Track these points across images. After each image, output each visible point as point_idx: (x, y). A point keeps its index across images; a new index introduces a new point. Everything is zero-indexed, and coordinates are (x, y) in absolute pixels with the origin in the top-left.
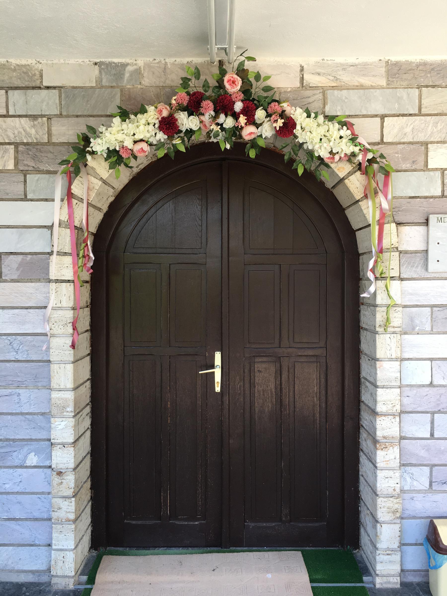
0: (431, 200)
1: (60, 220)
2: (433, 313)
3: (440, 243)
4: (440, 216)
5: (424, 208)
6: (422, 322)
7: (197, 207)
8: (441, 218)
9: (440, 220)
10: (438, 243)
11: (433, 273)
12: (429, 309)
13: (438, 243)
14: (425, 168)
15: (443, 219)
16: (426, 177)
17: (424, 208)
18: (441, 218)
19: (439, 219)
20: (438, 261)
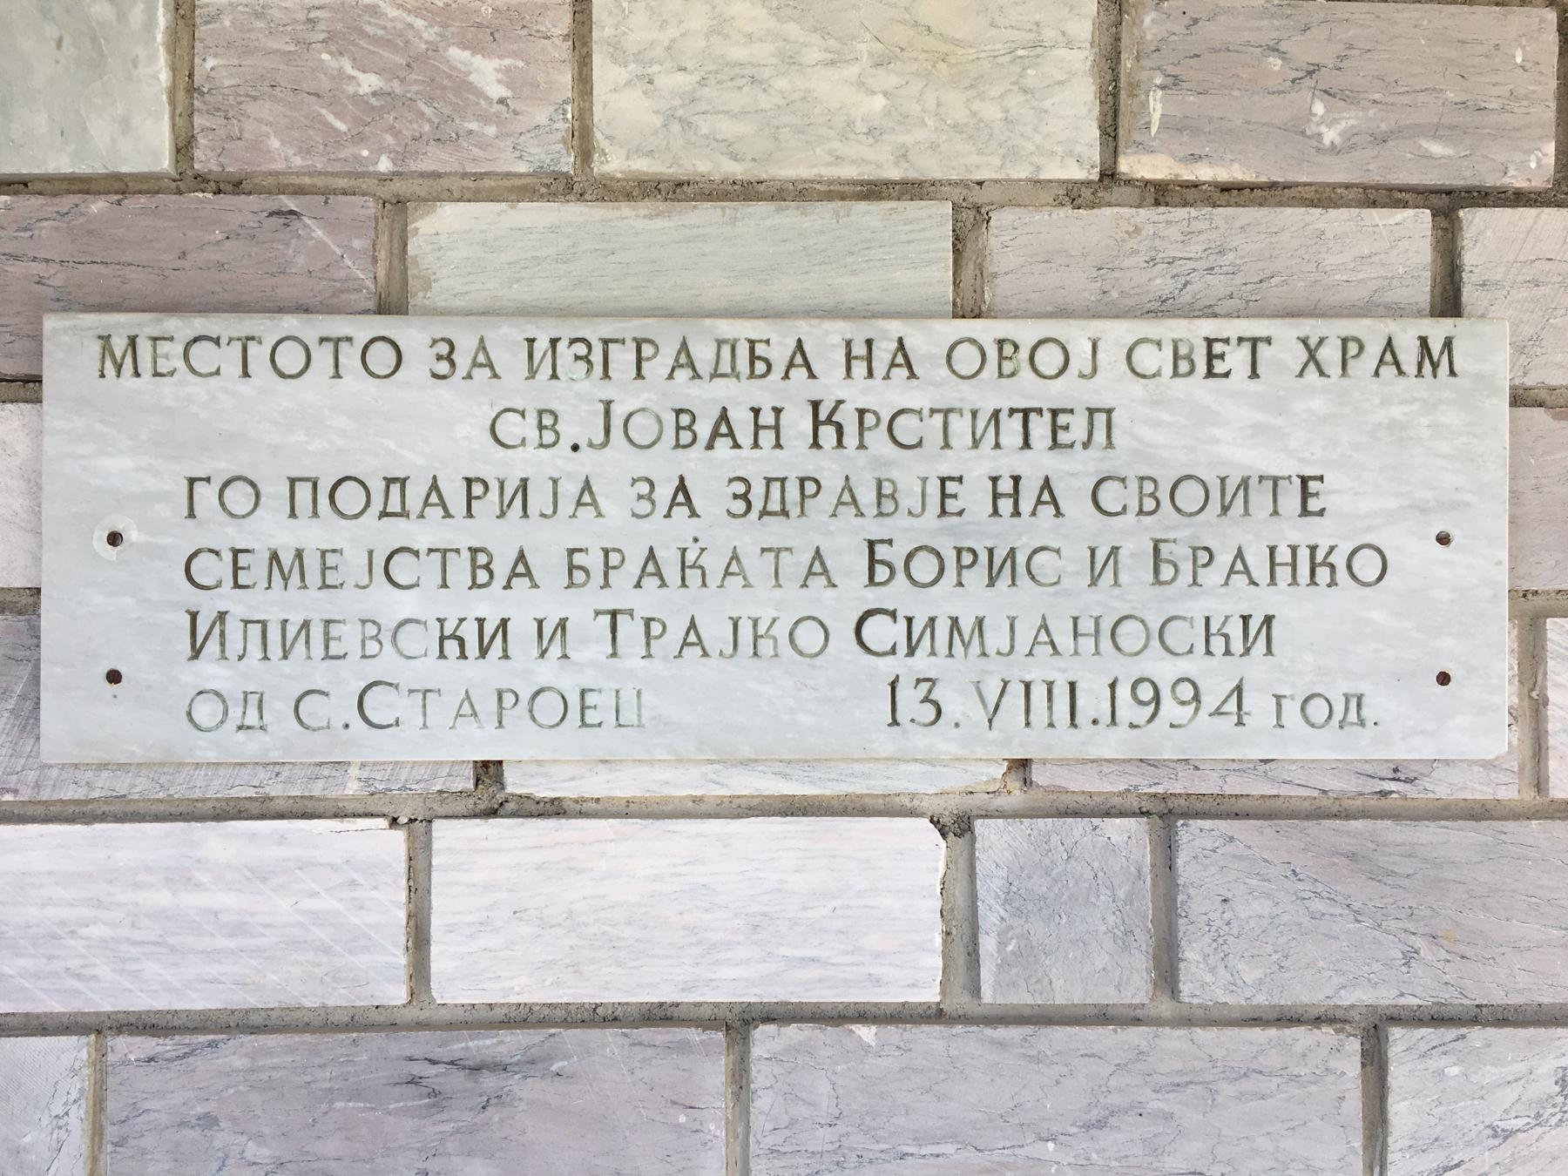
0: (97, 206)
1: (349, 763)
2: (112, 1082)
3: (132, 535)
4: (120, 324)
5: (37, 268)
6: (18, 1151)
7: (580, 708)
8: (133, 341)
9: (119, 358)
10: (114, 539)
11: (102, 766)
12: (73, 1050)
13: (114, 539)
14: (1529, 796)
15: (144, 348)
16: (52, 31)
17: (37, 268)
18: (133, 341)
19: (119, 344)
20: (114, 677)
